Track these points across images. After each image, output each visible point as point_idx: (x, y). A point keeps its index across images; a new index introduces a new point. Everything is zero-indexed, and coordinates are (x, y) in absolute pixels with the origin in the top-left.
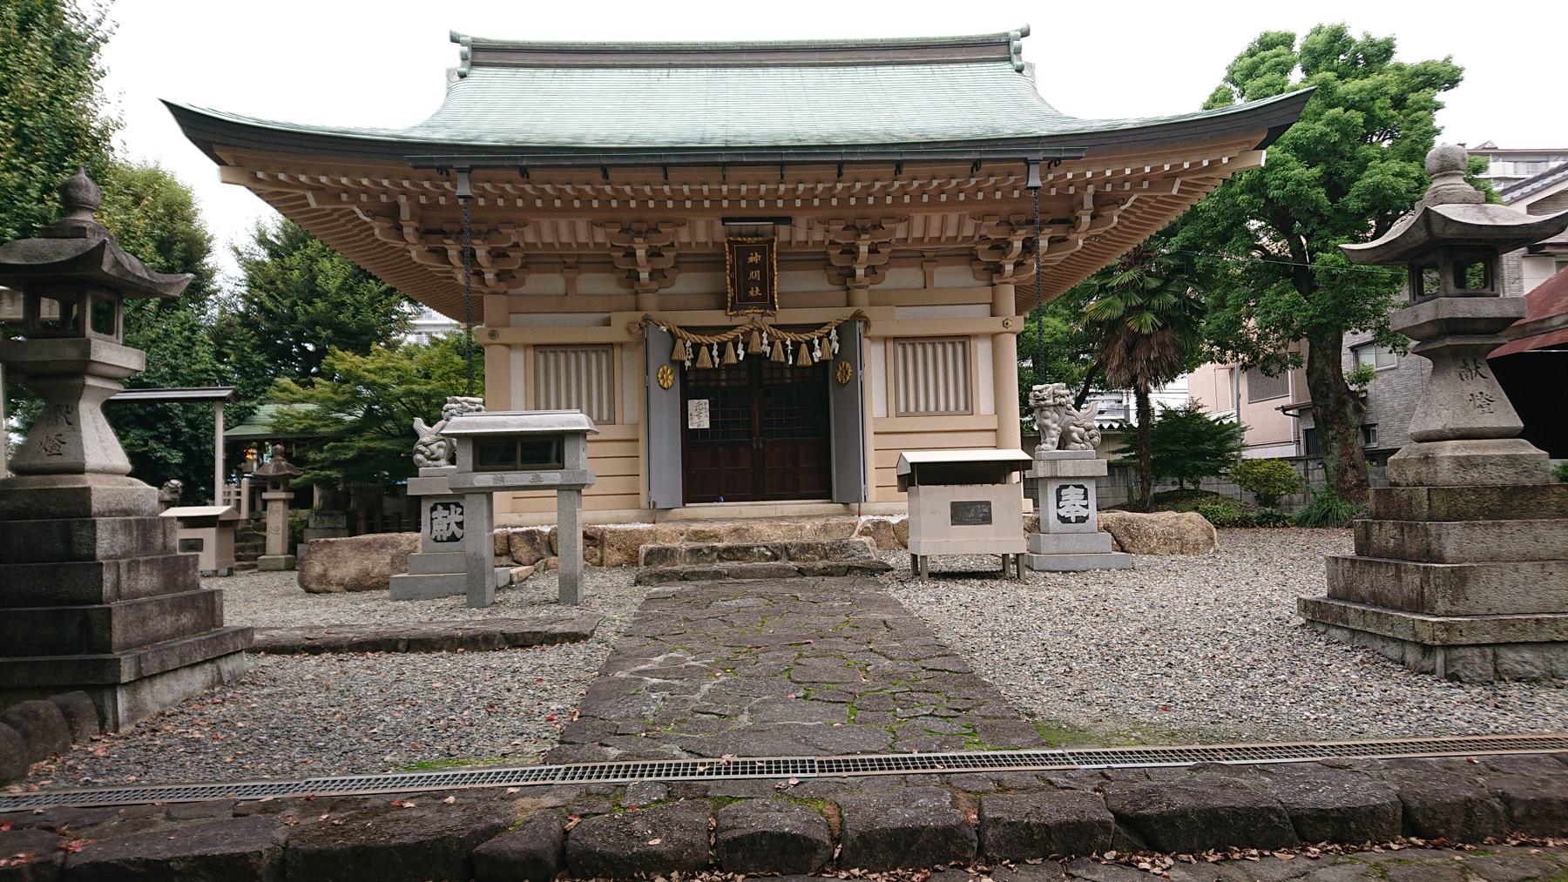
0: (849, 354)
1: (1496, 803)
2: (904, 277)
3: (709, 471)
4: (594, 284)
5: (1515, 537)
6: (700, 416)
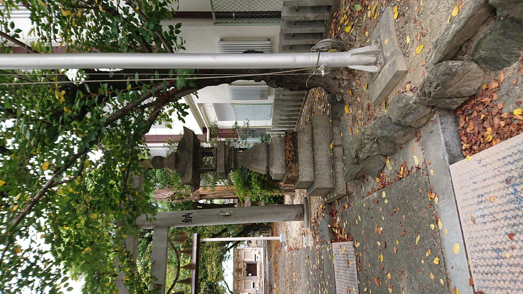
3: (254, 274)
6: (250, 275)
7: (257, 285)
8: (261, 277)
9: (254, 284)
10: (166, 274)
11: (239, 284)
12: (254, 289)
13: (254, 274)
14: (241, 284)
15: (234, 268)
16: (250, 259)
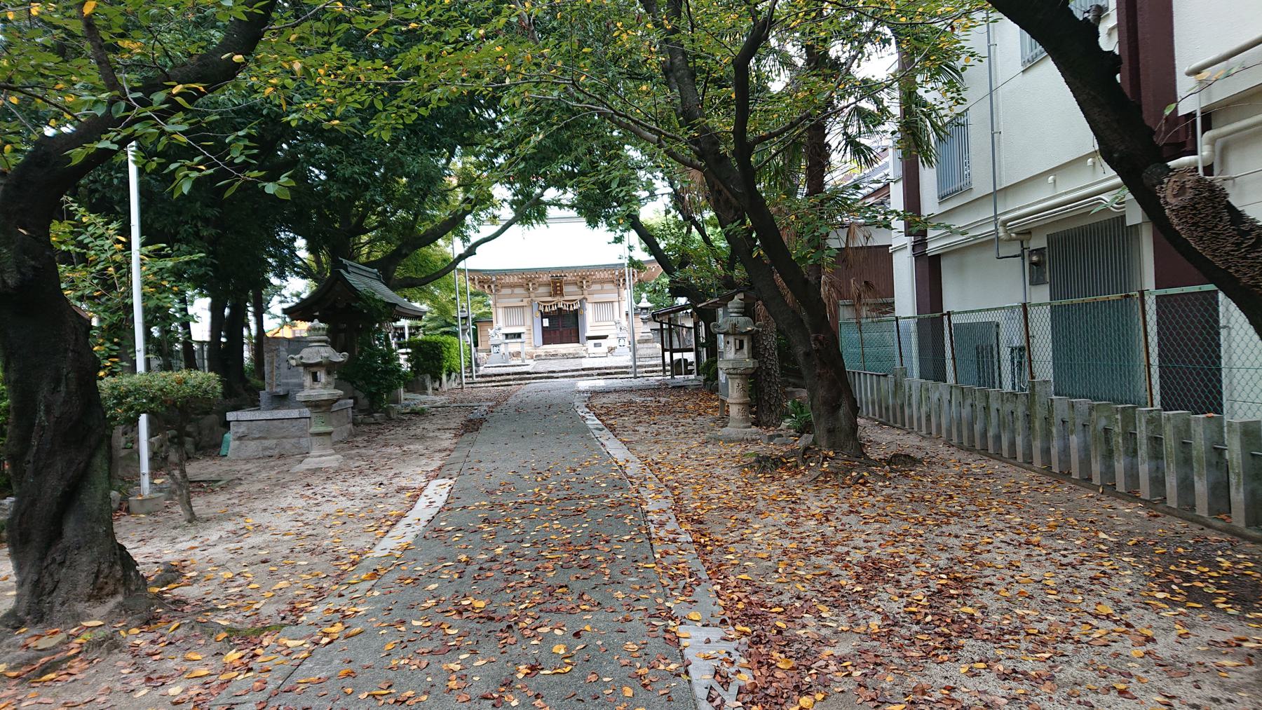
0: (582, 307)
1: (1151, 428)
2: (596, 287)
3: (549, 336)
4: (518, 291)
5: (646, 345)
6: (546, 323)
7: (514, 346)
9: (519, 335)
11: (517, 291)
12: (502, 338)
13: (549, 336)
14: (517, 296)
16: (591, 322)
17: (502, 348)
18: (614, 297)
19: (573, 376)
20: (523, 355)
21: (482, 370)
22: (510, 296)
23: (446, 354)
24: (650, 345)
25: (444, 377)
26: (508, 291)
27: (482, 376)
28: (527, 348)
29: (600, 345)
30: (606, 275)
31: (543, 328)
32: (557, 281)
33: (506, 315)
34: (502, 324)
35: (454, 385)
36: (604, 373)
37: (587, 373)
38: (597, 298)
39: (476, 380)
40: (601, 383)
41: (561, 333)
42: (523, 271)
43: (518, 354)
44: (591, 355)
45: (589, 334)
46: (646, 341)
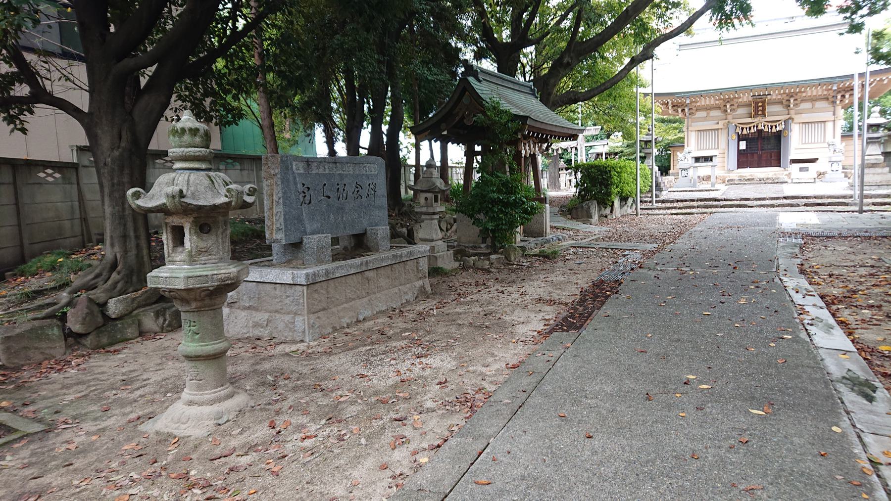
2: (805, 106)
3: (744, 160)
6: (743, 145)
7: (704, 169)
8: (731, 182)
9: (708, 159)
10: (161, 115)
11: (714, 113)
12: (691, 162)
13: (744, 160)
14: (713, 118)
15: (766, 87)
16: (796, 144)
17: (691, 171)
18: (828, 116)
19: (772, 206)
20: (713, 179)
21: (665, 195)
22: (705, 119)
23: (615, 179)
24: (879, 170)
25: (617, 203)
26: (703, 114)
27: (663, 202)
28: (719, 172)
29: (807, 169)
30: (820, 91)
31: (739, 151)
32: (758, 102)
33: (698, 140)
34: (693, 146)
35: (629, 211)
36: (815, 203)
37: (791, 202)
38: (805, 117)
39: (655, 205)
40: (811, 219)
41: (760, 157)
42: (720, 92)
43: (708, 178)
44: (790, 180)
45: (793, 156)
46: (874, 165)
